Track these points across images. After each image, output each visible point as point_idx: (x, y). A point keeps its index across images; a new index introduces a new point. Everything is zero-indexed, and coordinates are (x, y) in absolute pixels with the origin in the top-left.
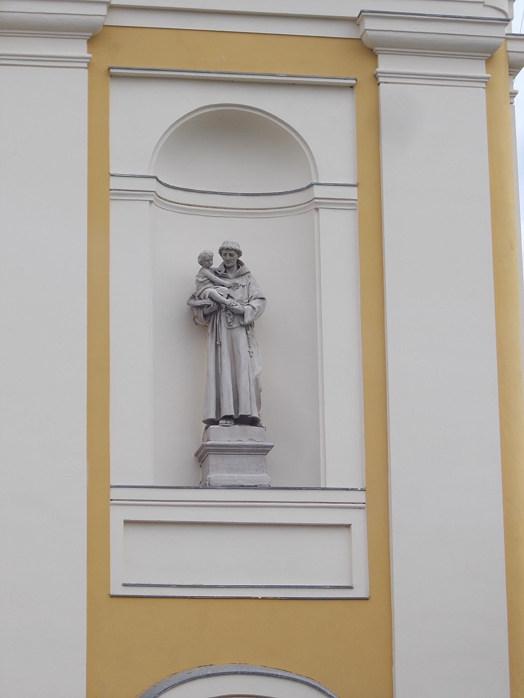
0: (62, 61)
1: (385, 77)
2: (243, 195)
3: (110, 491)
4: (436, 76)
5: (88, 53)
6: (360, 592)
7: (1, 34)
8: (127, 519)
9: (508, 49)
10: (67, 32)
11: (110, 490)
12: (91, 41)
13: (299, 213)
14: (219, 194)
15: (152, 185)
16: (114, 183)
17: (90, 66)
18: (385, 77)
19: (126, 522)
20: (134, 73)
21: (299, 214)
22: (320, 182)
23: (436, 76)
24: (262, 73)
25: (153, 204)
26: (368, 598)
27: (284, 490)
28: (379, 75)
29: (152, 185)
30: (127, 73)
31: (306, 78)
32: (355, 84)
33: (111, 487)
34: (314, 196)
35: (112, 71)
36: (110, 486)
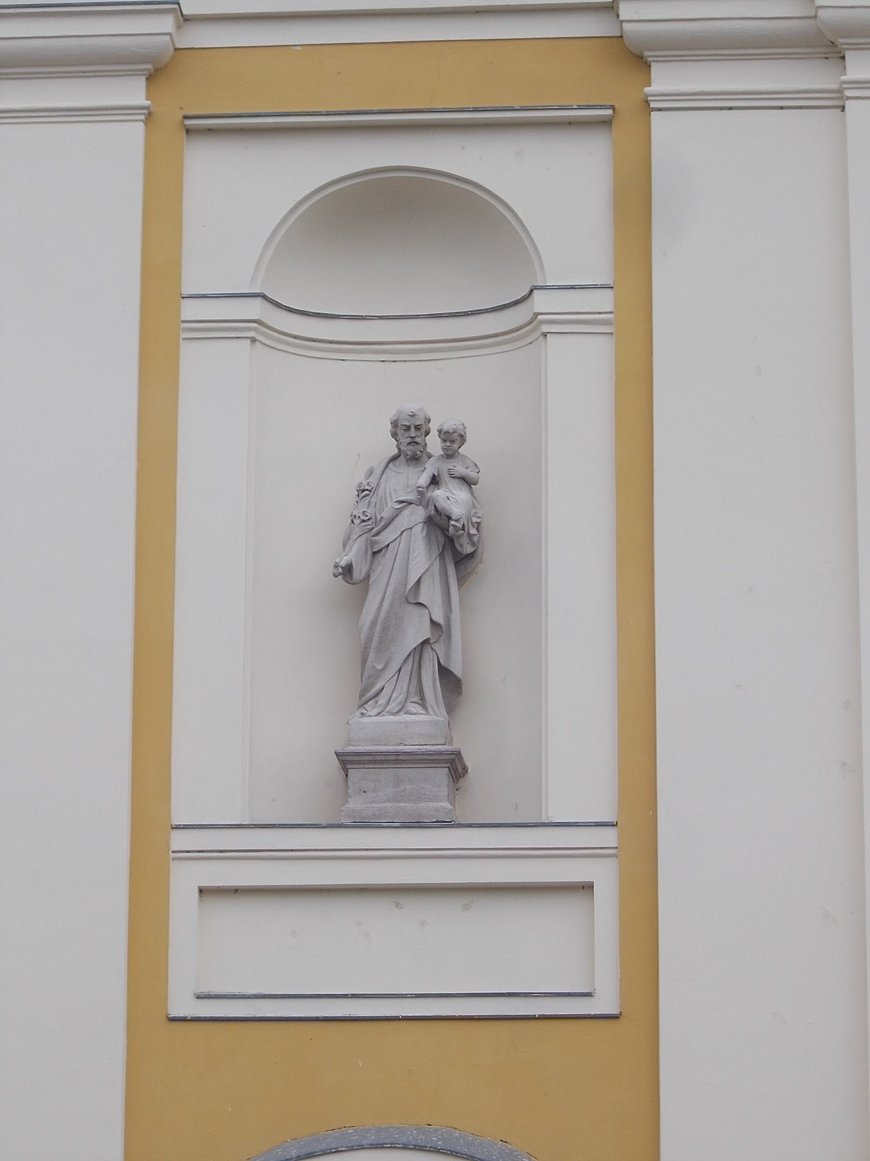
0: (733, 99)
1: (669, 100)
2: (381, 318)
3: (171, 834)
4: (660, 95)
5: (147, 99)
6: (604, 1004)
7: (2, 76)
8: (206, 883)
9: (178, 46)
10: (14, 67)
11: (170, 832)
12: (151, 78)
13: (530, 342)
14: (471, 314)
15: (254, 309)
16: (191, 310)
17: (149, 117)
18: (669, 100)
19: (201, 891)
20: (456, 119)
21: (529, 344)
22: (547, 285)
23: (660, 95)
24: (460, 108)
25: (258, 344)
26: (618, 1016)
27: (361, 829)
28: (650, 98)
29: (254, 309)
30: (227, 124)
31: (442, 113)
32: (613, 116)
33: (173, 828)
34: (533, 309)
35: (188, 122)
36: (171, 826)
